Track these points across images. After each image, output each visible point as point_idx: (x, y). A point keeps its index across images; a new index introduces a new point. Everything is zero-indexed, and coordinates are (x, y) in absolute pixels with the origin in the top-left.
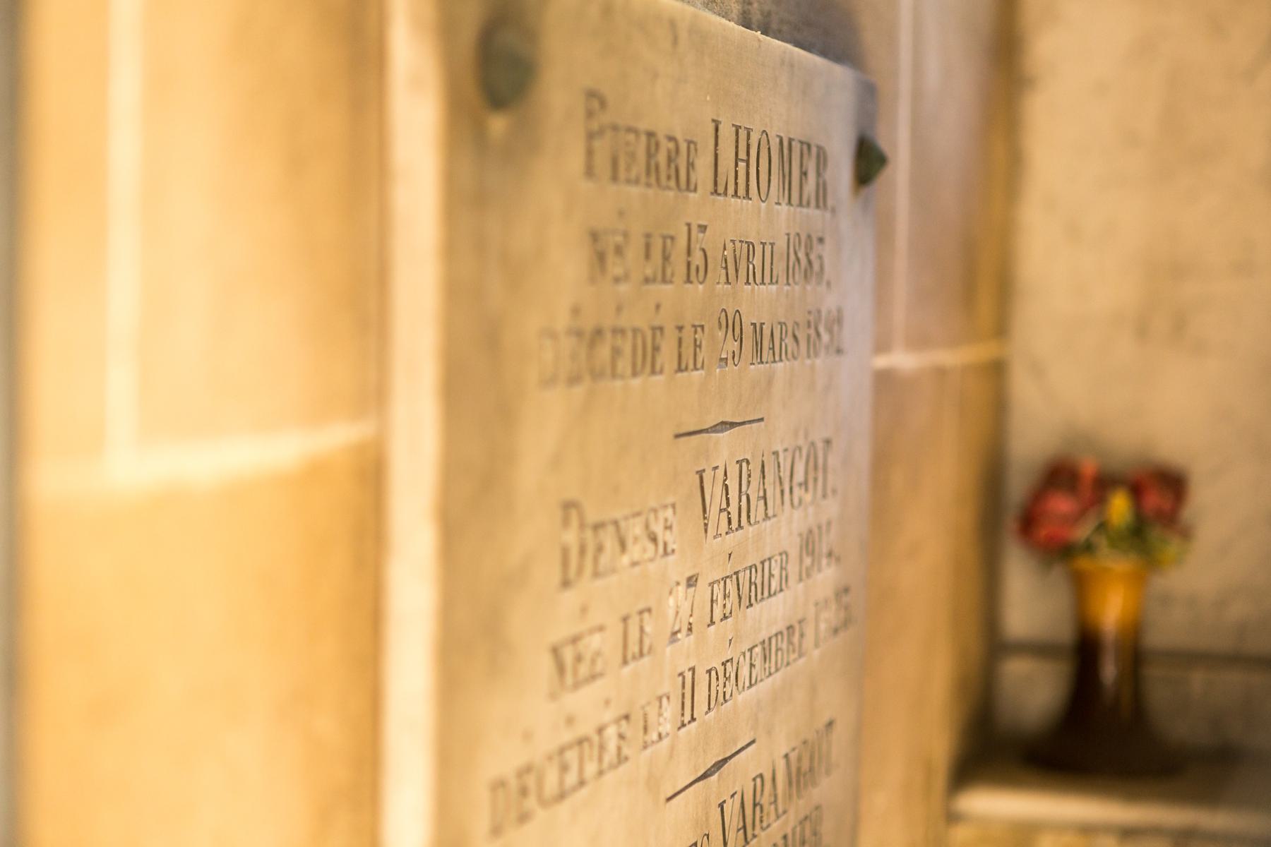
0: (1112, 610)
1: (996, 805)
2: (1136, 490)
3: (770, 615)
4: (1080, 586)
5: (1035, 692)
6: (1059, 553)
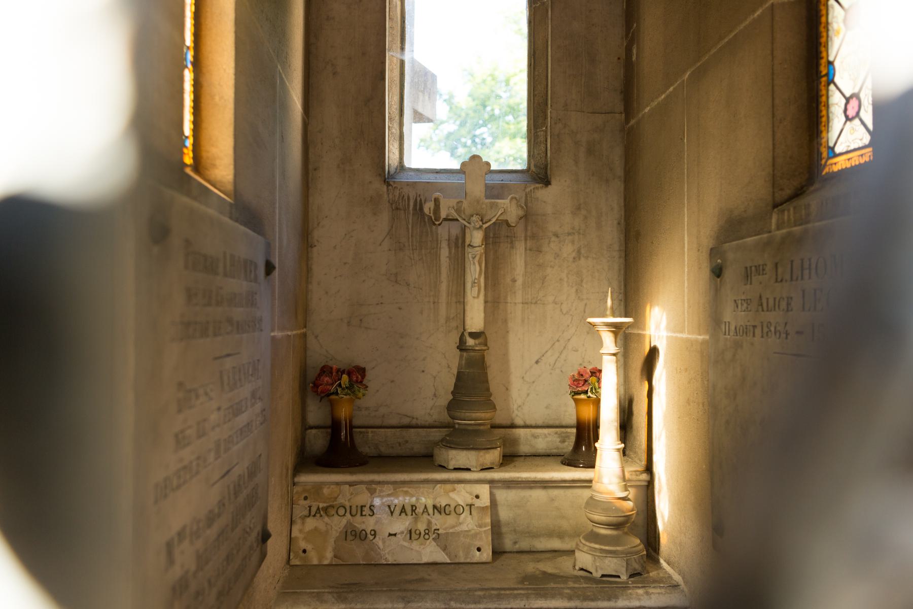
0: (343, 412)
1: (309, 479)
2: (349, 374)
3: (243, 419)
4: (332, 404)
5: (318, 441)
6: (326, 396)
